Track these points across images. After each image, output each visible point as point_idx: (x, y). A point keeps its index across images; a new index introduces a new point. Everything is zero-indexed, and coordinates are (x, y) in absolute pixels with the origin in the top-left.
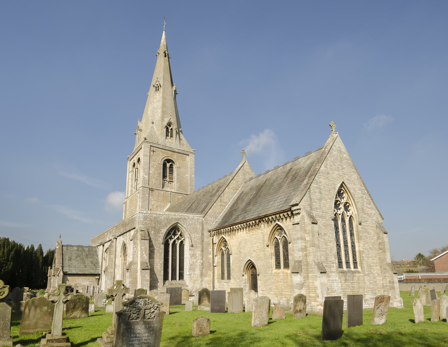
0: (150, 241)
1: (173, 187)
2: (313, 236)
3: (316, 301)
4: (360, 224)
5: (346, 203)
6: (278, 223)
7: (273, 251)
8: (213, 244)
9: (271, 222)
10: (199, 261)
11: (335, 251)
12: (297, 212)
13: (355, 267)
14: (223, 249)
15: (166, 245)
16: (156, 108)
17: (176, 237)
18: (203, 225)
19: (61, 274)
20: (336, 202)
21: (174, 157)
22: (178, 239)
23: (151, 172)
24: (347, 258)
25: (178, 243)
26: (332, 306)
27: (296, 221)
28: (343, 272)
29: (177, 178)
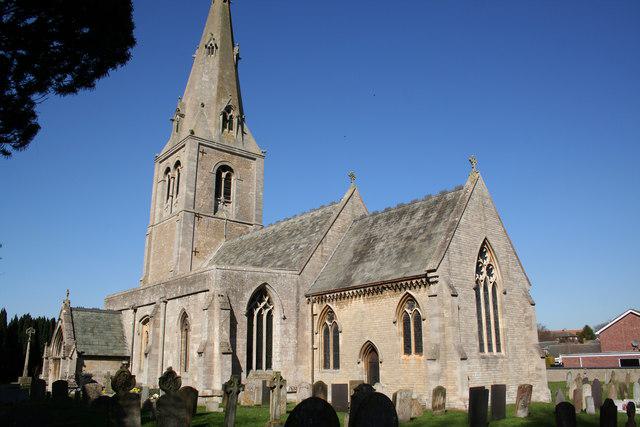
0: (232, 311)
1: (230, 211)
2: (453, 312)
3: (455, 395)
4: (505, 293)
5: (489, 265)
6: (410, 292)
7: (401, 330)
8: (313, 315)
9: (400, 290)
10: (293, 341)
11: (476, 330)
12: (434, 279)
13: (499, 350)
14: (329, 323)
15: (250, 315)
16: (204, 80)
17: (263, 304)
18: (298, 287)
19: (75, 356)
20: (478, 263)
21: (233, 162)
22: (265, 307)
23: (198, 186)
24: (489, 338)
25: (265, 313)
26: (477, 394)
27: (433, 293)
28: (483, 358)
29: (237, 198)
